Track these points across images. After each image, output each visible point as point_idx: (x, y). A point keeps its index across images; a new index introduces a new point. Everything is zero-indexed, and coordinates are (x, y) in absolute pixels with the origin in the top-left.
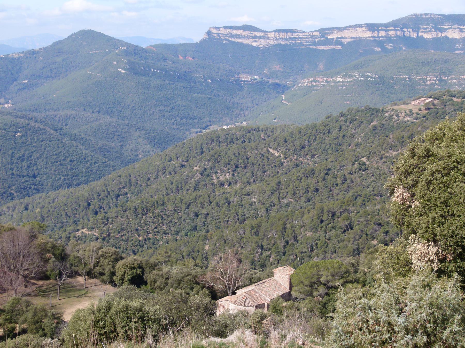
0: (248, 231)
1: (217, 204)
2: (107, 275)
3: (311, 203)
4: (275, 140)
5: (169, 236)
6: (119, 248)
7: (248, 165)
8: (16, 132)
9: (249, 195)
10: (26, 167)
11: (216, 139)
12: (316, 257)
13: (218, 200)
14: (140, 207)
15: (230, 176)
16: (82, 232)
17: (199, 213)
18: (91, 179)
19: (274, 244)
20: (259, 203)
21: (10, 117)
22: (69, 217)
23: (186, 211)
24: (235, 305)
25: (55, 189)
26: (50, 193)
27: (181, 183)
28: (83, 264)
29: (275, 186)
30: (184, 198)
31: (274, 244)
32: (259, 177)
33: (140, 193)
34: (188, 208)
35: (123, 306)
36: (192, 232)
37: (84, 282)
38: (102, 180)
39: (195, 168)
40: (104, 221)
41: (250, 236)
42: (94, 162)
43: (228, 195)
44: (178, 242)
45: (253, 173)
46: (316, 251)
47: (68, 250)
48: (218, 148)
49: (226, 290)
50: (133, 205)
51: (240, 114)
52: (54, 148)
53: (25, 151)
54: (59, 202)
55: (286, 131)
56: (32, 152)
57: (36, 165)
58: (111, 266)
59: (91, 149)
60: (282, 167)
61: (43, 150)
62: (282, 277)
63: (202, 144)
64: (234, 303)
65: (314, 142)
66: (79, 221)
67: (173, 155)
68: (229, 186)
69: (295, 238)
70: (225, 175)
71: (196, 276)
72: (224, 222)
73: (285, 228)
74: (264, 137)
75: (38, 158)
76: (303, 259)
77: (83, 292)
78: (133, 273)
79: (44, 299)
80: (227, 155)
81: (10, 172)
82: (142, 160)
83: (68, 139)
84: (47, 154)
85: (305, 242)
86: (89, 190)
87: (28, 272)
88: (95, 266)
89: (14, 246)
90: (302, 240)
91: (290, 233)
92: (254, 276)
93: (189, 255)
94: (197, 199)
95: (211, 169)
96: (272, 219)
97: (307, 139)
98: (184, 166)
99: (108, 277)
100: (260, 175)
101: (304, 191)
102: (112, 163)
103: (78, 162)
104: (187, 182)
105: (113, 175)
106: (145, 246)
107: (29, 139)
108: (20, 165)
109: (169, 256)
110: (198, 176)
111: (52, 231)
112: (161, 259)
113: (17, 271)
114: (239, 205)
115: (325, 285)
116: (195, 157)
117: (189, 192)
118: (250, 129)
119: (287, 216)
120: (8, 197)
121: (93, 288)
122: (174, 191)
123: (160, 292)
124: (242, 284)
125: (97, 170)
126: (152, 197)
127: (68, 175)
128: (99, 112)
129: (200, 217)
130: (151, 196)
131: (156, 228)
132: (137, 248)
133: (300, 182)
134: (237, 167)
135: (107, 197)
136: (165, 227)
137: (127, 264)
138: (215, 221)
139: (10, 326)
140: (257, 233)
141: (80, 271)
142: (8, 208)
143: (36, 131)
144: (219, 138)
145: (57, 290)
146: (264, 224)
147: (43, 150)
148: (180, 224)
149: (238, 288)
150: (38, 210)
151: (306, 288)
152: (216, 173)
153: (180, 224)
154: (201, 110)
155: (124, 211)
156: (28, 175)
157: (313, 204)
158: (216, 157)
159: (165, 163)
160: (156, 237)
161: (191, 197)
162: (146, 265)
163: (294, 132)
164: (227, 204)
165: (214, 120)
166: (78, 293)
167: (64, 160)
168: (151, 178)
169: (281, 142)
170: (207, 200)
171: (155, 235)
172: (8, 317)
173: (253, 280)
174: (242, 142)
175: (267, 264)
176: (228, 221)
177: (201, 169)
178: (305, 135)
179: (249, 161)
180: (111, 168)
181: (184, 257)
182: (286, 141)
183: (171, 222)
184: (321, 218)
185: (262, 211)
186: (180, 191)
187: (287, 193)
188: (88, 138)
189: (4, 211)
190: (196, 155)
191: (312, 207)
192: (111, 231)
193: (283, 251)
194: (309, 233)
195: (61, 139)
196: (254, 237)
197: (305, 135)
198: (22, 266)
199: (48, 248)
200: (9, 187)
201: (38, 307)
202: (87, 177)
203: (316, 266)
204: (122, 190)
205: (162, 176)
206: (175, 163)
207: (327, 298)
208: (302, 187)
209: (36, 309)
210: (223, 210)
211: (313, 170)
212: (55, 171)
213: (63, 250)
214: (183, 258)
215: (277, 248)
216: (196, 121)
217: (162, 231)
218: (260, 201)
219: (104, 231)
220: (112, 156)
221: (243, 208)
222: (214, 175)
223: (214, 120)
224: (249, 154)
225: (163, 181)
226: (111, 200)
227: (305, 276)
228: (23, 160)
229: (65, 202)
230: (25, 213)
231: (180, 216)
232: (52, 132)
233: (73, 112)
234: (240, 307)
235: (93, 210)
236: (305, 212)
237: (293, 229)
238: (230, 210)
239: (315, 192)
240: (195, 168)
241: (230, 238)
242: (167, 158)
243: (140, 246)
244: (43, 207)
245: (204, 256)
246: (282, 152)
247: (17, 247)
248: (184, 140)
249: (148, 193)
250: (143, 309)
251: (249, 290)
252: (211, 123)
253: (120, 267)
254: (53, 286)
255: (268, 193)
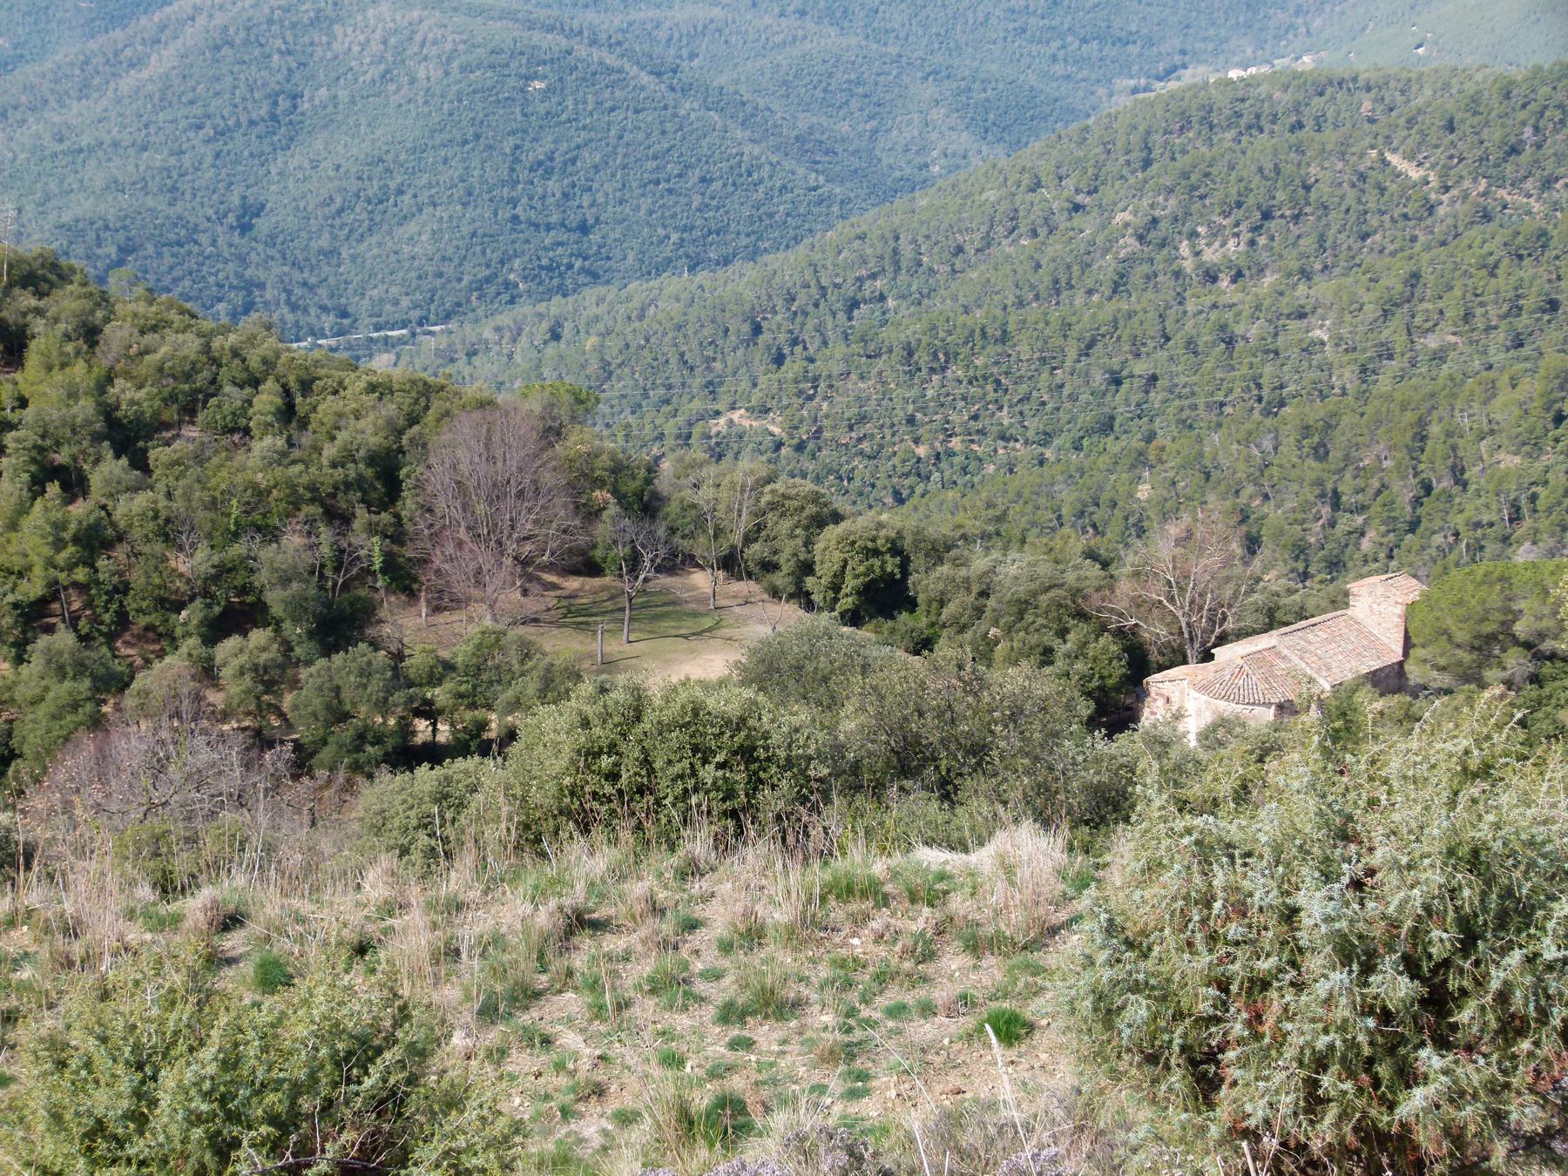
0: (1288, 444)
1: (1189, 343)
2: (786, 569)
3: (1526, 351)
4: (1411, 122)
5: (1018, 446)
6: (850, 480)
7: (1308, 210)
8: (528, 78)
9: (1302, 316)
10: (558, 195)
11: (1198, 117)
12: (1527, 544)
13: (1194, 332)
14: (924, 342)
15: (1242, 247)
16: (731, 421)
17: (1124, 373)
18: (767, 245)
19: (1379, 492)
20: (1337, 345)
21: (510, 25)
22: (692, 369)
23: (1079, 366)
24: (1205, 698)
25: (649, 273)
26: (630, 286)
27: (1069, 267)
28: (711, 532)
29: (1399, 287)
30: (1073, 319)
31: (1379, 492)
32: (1343, 256)
33: (928, 296)
34: (1087, 355)
35: (683, 707)
36: (1095, 438)
37: (710, 591)
38: (802, 249)
39: (1120, 218)
40: (802, 386)
41: (1295, 460)
42: (779, 184)
43: (1229, 315)
44: (1045, 468)
45: (1322, 239)
46: (1528, 522)
47: (663, 484)
48: (1204, 149)
49: (1181, 645)
50: (902, 337)
51: (1291, 26)
52: (648, 135)
53: (555, 142)
54: (660, 316)
55: (1454, 91)
56: (578, 147)
57: (590, 189)
58: (800, 542)
59: (772, 141)
60: (1429, 221)
61: (613, 141)
62: (1376, 614)
63: (1148, 133)
64: (1204, 688)
65: (1556, 131)
66: (722, 383)
67: (1045, 169)
68: (1234, 281)
69: (1458, 474)
70: (1223, 244)
71: (1079, 590)
72: (1208, 407)
73: (1423, 438)
74: (1373, 110)
75: (596, 168)
76: (1482, 548)
77: (708, 622)
78: (870, 569)
79: (581, 637)
80: (1234, 174)
81: (505, 213)
82: (940, 182)
83: (696, 105)
84: (625, 156)
85: (1491, 487)
86: (758, 282)
87: (533, 547)
88: (748, 540)
89: (491, 459)
90: (1483, 482)
91: (1439, 455)
92: (1283, 601)
93: (1081, 514)
94: (1121, 323)
95: (1176, 220)
96: (1377, 403)
97: (1532, 121)
98: (1084, 207)
99: (791, 579)
100: (1350, 248)
101: (1505, 308)
102: (838, 190)
103: (725, 185)
104: (1089, 266)
105: (841, 231)
106: (936, 476)
107: (570, 103)
108: (540, 190)
109: (1000, 519)
110: (1129, 244)
111: (633, 413)
112: (973, 526)
113: (499, 543)
114: (1267, 352)
115: (1528, 646)
116: (1122, 177)
117: (1096, 298)
118: (1323, 80)
119: (1432, 395)
120: (499, 294)
121: (737, 609)
122: (1044, 294)
123: (960, 637)
124: (1237, 626)
125: (788, 215)
126: (966, 310)
127: (692, 228)
128: (802, 13)
129: (1125, 386)
130: (965, 307)
131: (975, 417)
132: (907, 482)
133: (1492, 275)
134: (1267, 216)
135: (816, 305)
136: (1005, 417)
137: (852, 538)
138: (1177, 403)
139: (469, 715)
140: (1322, 451)
141: (697, 552)
142: (498, 329)
143: (594, 74)
144: (1211, 111)
145: (622, 610)
146: (1346, 420)
147: (613, 141)
148: (1058, 409)
149: (1222, 640)
150: (591, 342)
151: (1459, 652)
152: (1193, 234)
153: (1058, 409)
154: (1153, 10)
155: (869, 357)
156: (563, 225)
157: (1535, 354)
158: (1194, 178)
159: (1018, 199)
160: (975, 447)
161: (1101, 317)
162: (916, 543)
163: (1486, 93)
164: (1223, 346)
165: (1199, 46)
166: (689, 624)
167: (680, 176)
168: (967, 248)
169: (1434, 128)
170: (1153, 330)
171: (972, 441)
172: (463, 688)
173: (1278, 615)
174: (1292, 129)
175: (1351, 558)
176: (1222, 405)
177: (1139, 221)
178: (1524, 106)
179: (1313, 195)
180: (835, 209)
181: (1064, 520)
182: (1451, 127)
183: (1026, 399)
184: (1556, 406)
185: (1347, 375)
186: (1065, 294)
187: (1441, 312)
188: (761, 103)
189: (486, 342)
190: (1124, 172)
191: (1528, 365)
192: (826, 422)
193: (1408, 518)
194: (1509, 457)
195: (672, 103)
196: (1311, 462)
197: (1524, 106)
198: (512, 527)
199: (598, 473)
200: (502, 262)
201: (557, 662)
202: (753, 238)
203: (1501, 579)
204: (867, 284)
205: (1004, 242)
206: (1053, 198)
207: (1534, 694)
208: (1497, 293)
209: (549, 668)
210: (1208, 366)
211: (1543, 234)
212: (651, 212)
213: (648, 481)
214: (1062, 525)
215: (1388, 505)
216: (1134, 49)
217: (995, 428)
218: (1341, 339)
219: (801, 422)
220: (838, 168)
221: (1278, 362)
222: (1185, 243)
223: (1199, 46)
224: (1312, 170)
225: (1008, 258)
226: (829, 318)
227: (1461, 611)
228: (548, 173)
229: (678, 319)
230: (551, 350)
231: (1058, 380)
232: (645, 78)
233: (717, 12)
234: (1222, 704)
235: (769, 348)
236: (1499, 384)
237: (1451, 440)
238: (1233, 369)
239: (1544, 311)
240: (1120, 218)
241: (1225, 462)
242: (1026, 180)
243: (919, 475)
244: (609, 332)
245: (1131, 520)
246: (1433, 167)
247: (499, 464)
248: (1088, 116)
249: (955, 298)
250: (751, 722)
251: (1260, 647)
252: (1187, 59)
253: (828, 547)
254: (612, 598)
255: (1371, 312)
